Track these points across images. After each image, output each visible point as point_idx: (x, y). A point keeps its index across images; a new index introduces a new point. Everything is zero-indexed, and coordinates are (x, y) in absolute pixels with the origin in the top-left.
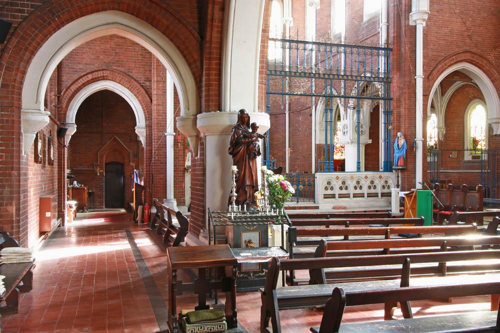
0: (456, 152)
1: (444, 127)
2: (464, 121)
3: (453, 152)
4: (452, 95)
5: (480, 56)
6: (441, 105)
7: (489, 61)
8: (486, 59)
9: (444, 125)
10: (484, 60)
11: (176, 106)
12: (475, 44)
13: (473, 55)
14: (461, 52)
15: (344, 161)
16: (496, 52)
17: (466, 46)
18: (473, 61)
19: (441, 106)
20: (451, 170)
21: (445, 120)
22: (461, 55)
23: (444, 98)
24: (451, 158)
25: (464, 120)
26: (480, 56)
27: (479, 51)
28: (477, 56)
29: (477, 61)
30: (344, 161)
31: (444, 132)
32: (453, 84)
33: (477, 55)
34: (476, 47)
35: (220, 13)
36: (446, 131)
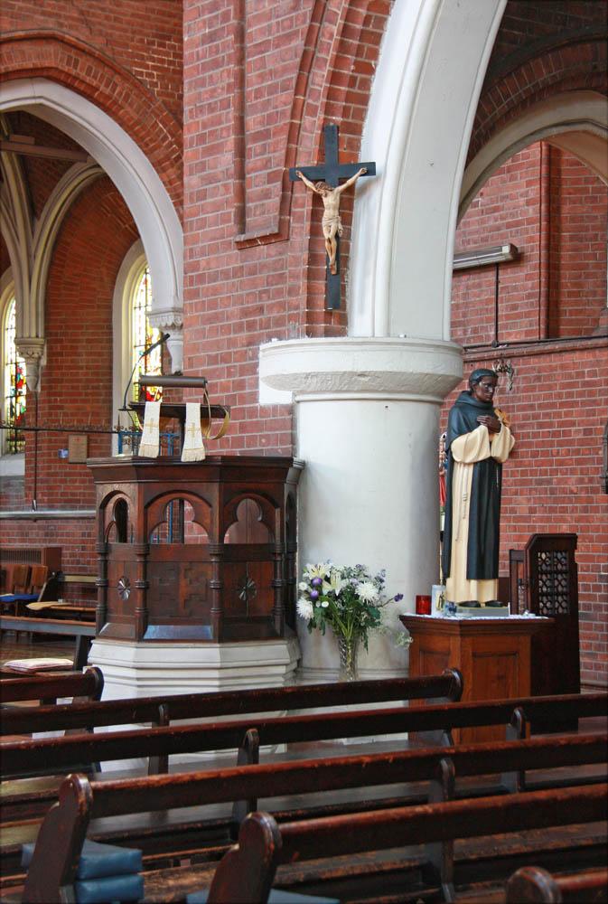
0: (84, 439)
1: (41, 340)
2: (109, 320)
3: (72, 439)
4: (63, 223)
5: (101, 61)
6: (29, 255)
7: (139, 85)
8: (127, 76)
9: (41, 334)
10: (117, 79)
11: (175, 189)
12: (82, 13)
13: (73, 53)
14: (22, 33)
15: (374, 163)
16: (167, 54)
17: (44, 14)
18: (75, 78)
19: (31, 257)
20: (63, 508)
21: (47, 314)
22: (26, 47)
23: (39, 224)
24: (66, 460)
25: (111, 313)
26: (101, 61)
27: (97, 44)
28: (90, 63)
29: (88, 79)
30: (374, 163)
31: (44, 362)
32: (65, 171)
33: (90, 54)
34: (87, 22)
35: (238, 159)
36: (49, 355)
